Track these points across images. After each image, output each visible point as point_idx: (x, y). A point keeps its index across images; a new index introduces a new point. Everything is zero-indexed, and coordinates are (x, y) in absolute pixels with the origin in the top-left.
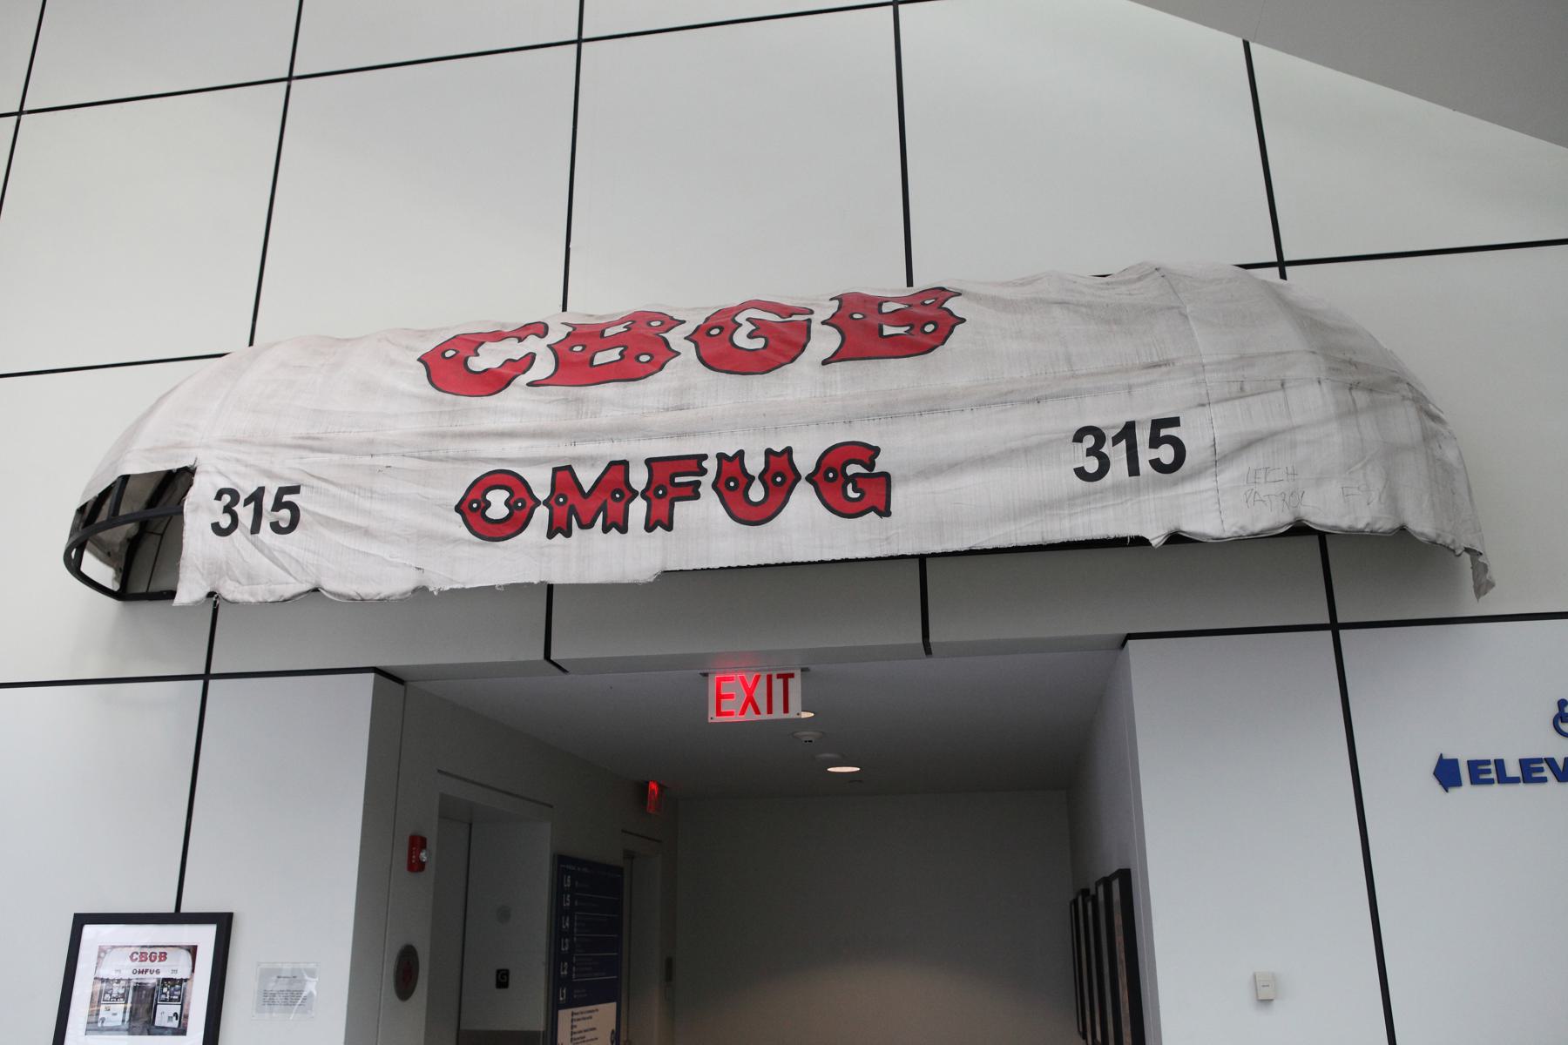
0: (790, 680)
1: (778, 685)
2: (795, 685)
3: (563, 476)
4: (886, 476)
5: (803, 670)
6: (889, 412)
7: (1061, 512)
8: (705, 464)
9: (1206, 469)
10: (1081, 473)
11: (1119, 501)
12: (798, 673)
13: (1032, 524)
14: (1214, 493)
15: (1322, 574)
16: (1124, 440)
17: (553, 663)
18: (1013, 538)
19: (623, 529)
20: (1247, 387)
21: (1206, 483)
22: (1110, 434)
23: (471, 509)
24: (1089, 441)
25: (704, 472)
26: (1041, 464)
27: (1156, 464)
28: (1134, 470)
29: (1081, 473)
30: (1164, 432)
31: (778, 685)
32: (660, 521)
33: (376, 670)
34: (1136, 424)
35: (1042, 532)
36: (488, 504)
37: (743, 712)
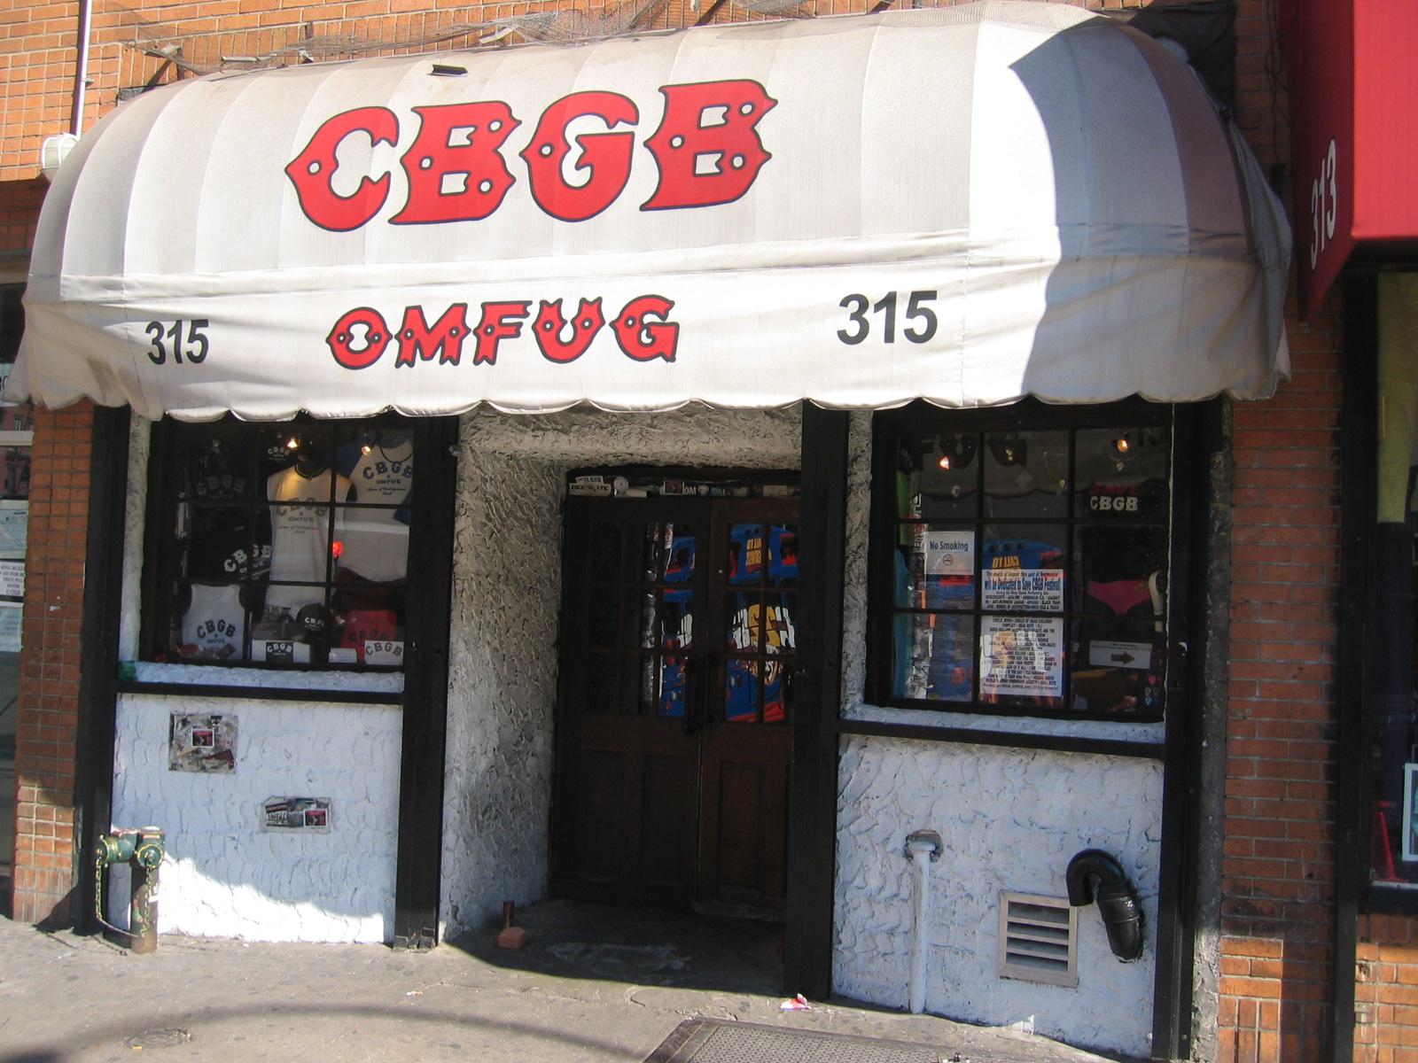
4: (676, 326)
10: (843, 336)
21: (952, 355)
23: (338, 338)
25: (526, 315)
27: (910, 334)
28: (889, 337)
29: (843, 336)
32: (486, 355)
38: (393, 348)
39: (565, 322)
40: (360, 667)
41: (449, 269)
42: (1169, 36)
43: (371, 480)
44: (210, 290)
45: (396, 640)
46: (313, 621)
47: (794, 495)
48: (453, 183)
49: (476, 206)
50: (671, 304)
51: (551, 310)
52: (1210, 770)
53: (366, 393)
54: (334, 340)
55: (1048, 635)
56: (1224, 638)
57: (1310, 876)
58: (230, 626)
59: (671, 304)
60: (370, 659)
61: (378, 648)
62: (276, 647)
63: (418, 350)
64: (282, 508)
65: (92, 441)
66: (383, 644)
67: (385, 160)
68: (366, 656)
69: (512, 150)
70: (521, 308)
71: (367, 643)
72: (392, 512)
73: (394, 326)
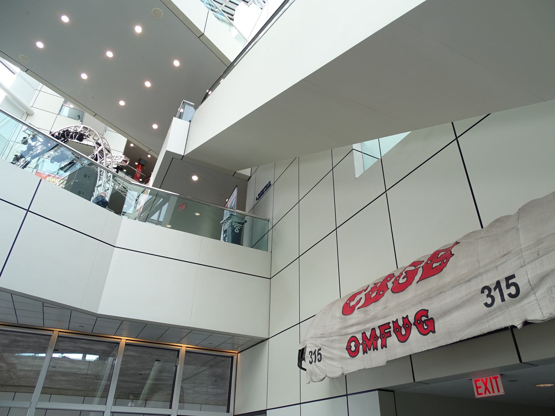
0: (497, 379)
1: (494, 381)
2: (499, 380)
4: (432, 319)
5: (501, 375)
6: (429, 297)
7: (484, 321)
9: (530, 292)
10: (486, 305)
11: (502, 312)
12: (499, 376)
13: (476, 327)
14: (535, 302)
15: (514, 345)
16: (498, 288)
17: (523, 363)
18: (472, 335)
19: (377, 350)
20: (540, 253)
21: (532, 298)
22: (492, 287)
24: (486, 292)
25: (390, 328)
26: (474, 304)
27: (510, 295)
28: (503, 300)
29: (486, 305)
30: (510, 282)
31: (494, 381)
32: (403, 339)
33: (379, 390)
34: (500, 281)
35: (480, 330)
37: (485, 393)
43: (495, 304)
51: (395, 323)
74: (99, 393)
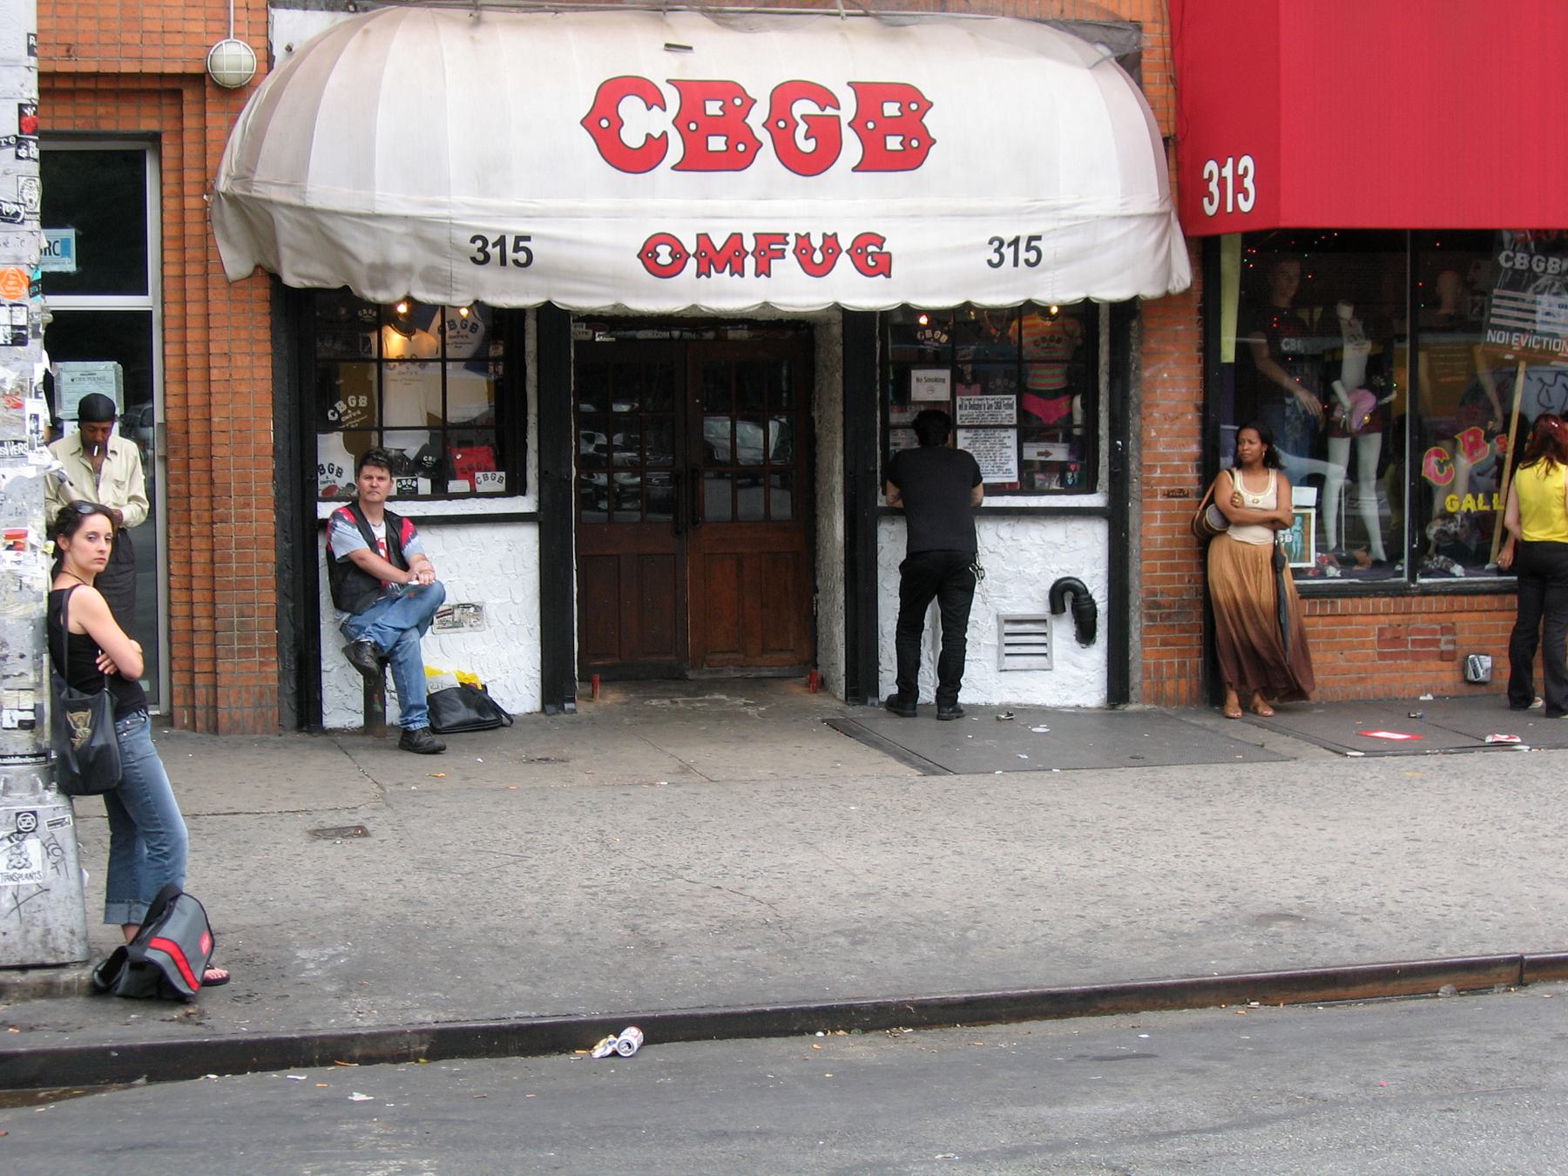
3: (703, 239)
4: (889, 254)
8: (788, 239)
10: (990, 262)
21: (1049, 274)
23: (647, 255)
24: (479, 243)
25: (787, 243)
28: (1016, 264)
29: (990, 262)
30: (522, 244)
32: (763, 270)
36: (658, 255)
38: (692, 264)
39: (815, 250)
40: (473, 494)
41: (723, 204)
42: (1103, 43)
44: (530, 213)
45: (498, 470)
46: (430, 458)
47: (753, 337)
48: (717, 143)
49: (738, 159)
50: (884, 239)
52: (1133, 521)
53: (676, 296)
54: (643, 255)
55: (1005, 441)
56: (1139, 438)
57: (1189, 582)
58: (339, 468)
59: (884, 239)
60: (480, 489)
61: (486, 478)
62: (404, 483)
63: (728, 266)
64: (392, 364)
65: (270, 313)
66: (489, 474)
67: (661, 122)
68: (477, 485)
69: (757, 119)
70: (782, 238)
71: (478, 475)
72: (464, 363)
73: (691, 246)
74: (1352, 542)
